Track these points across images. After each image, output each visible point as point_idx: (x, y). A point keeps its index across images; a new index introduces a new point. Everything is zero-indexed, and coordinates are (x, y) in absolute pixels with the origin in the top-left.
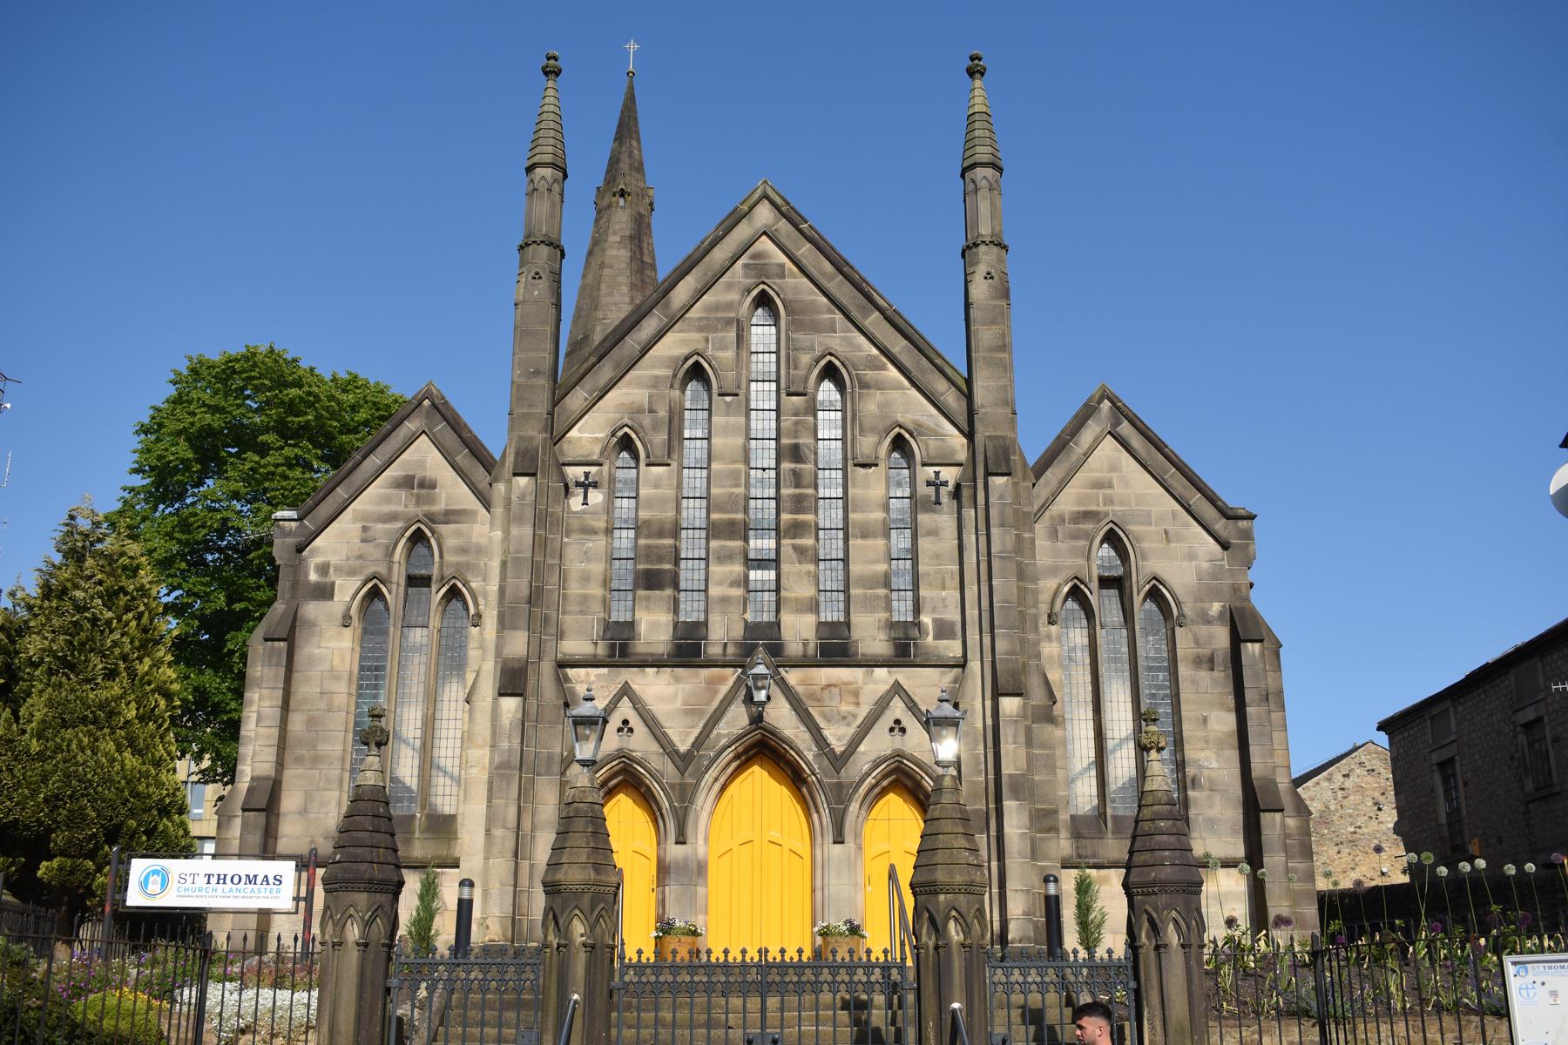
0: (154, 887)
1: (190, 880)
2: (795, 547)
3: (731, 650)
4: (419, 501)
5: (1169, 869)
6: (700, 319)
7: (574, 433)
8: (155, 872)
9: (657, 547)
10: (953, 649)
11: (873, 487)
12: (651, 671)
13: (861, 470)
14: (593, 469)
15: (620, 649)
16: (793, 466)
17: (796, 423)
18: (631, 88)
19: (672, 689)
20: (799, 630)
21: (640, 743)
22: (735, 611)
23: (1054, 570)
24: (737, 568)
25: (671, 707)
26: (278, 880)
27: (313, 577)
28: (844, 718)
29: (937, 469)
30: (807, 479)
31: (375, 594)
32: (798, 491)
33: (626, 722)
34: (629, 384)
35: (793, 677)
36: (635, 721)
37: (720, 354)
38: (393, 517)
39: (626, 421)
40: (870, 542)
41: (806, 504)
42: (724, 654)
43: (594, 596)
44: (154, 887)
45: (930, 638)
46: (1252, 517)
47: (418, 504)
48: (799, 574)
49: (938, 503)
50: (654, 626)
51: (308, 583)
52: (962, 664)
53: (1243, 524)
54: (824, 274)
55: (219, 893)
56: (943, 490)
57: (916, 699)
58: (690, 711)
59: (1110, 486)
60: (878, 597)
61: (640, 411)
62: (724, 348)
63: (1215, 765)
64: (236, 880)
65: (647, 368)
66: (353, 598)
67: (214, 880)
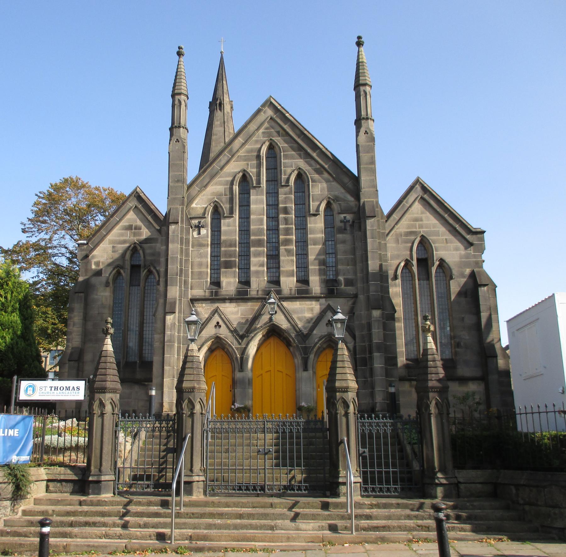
0: (30, 391)
1: (44, 389)
2: (286, 250)
3: (260, 293)
4: (135, 235)
5: (434, 382)
8: (30, 386)
10: (350, 290)
16: (284, 216)
17: (285, 198)
18: (222, 59)
19: (236, 309)
23: (397, 257)
26: (78, 388)
27: (93, 267)
31: (119, 273)
32: (287, 226)
33: (218, 323)
34: (216, 184)
35: (285, 304)
36: (221, 323)
38: (124, 242)
42: (257, 295)
44: (30, 391)
45: (343, 287)
46: (484, 232)
47: (134, 236)
48: (288, 260)
49: (345, 229)
50: (229, 283)
51: (92, 269)
52: (356, 296)
53: (479, 236)
55: (55, 394)
59: (421, 220)
61: (221, 195)
63: (467, 338)
64: (62, 389)
65: (221, 177)
66: (110, 275)
67: (53, 389)
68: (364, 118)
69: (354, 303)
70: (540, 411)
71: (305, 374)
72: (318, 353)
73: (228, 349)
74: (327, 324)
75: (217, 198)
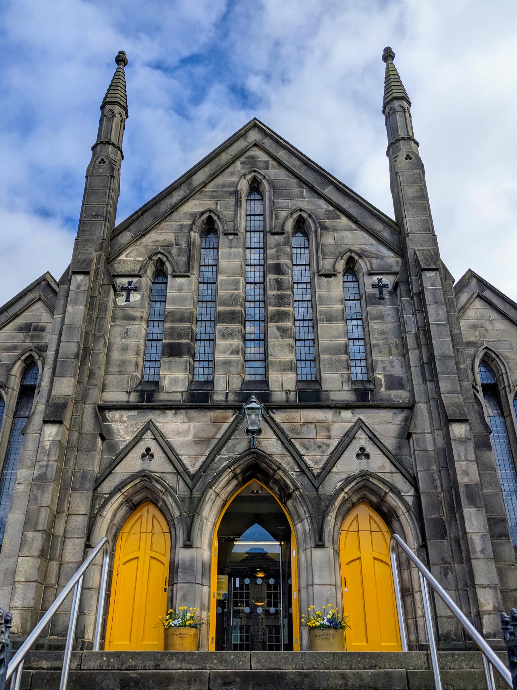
4: (32, 337)
6: (213, 192)
7: (122, 257)
9: (178, 328)
10: (400, 396)
11: (335, 290)
12: (170, 413)
13: (325, 279)
14: (135, 280)
15: (148, 398)
16: (276, 277)
19: (185, 426)
20: (283, 383)
21: (159, 465)
22: (235, 370)
24: (236, 342)
25: (185, 439)
28: (319, 447)
29: (379, 277)
30: (285, 286)
32: (279, 292)
33: (148, 450)
35: (279, 417)
37: (225, 212)
38: (15, 348)
39: (160, 250)
40: (333, 325)
41: (285, 300)
42: (226, 401)
43: (130, 361)
45: (383, 389)
48: (282, 346)
49: (382, 298)
52: (409, 407)
54: (234, 445)
56: (385, 291)
57: (376, 433)
58: (199, 442)
60: (341, 361)
62: (227, 208)
68: (403, 139)
69: (408, 420)
70: (315, 586)
71: (318, 554)
72: (345, 512)
73: (164, 501)
74: (358, 455)
75: (163, 249)
